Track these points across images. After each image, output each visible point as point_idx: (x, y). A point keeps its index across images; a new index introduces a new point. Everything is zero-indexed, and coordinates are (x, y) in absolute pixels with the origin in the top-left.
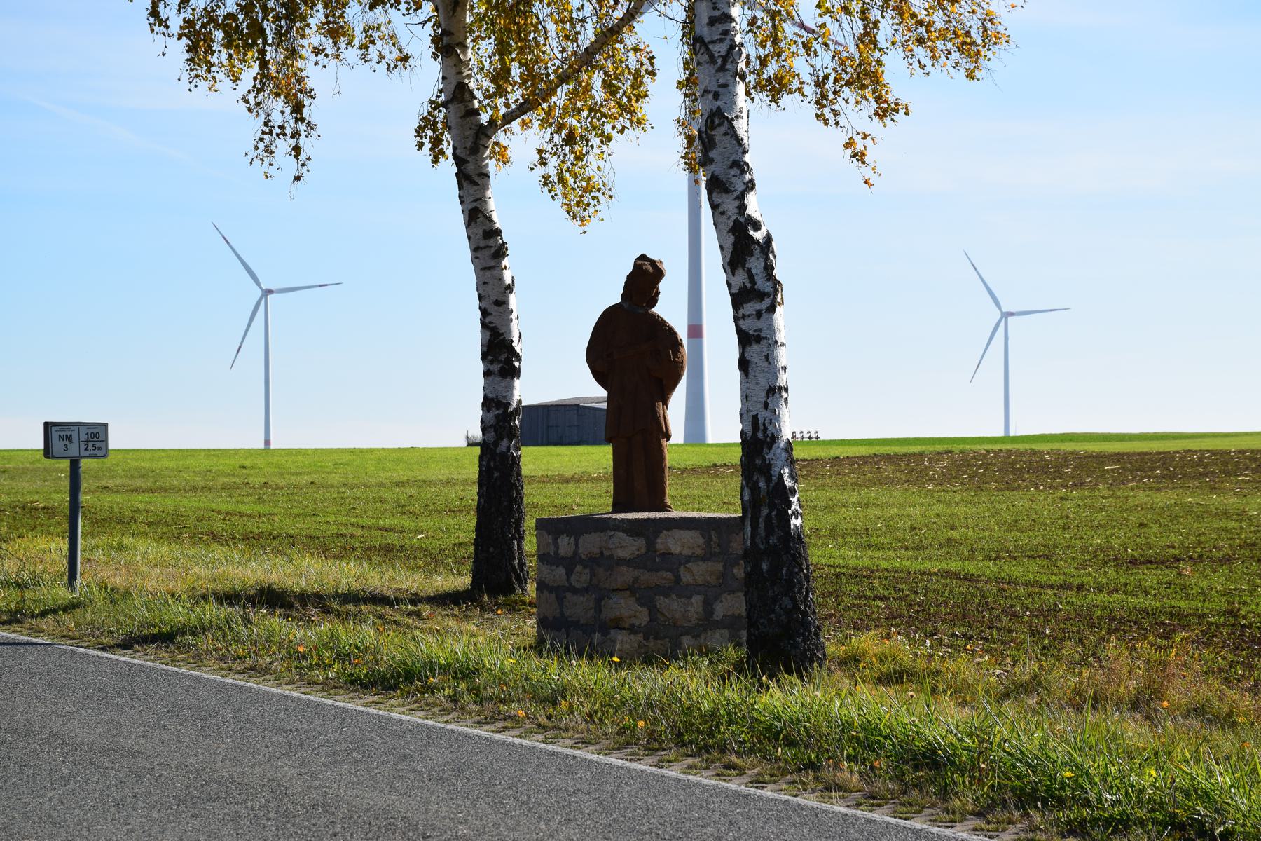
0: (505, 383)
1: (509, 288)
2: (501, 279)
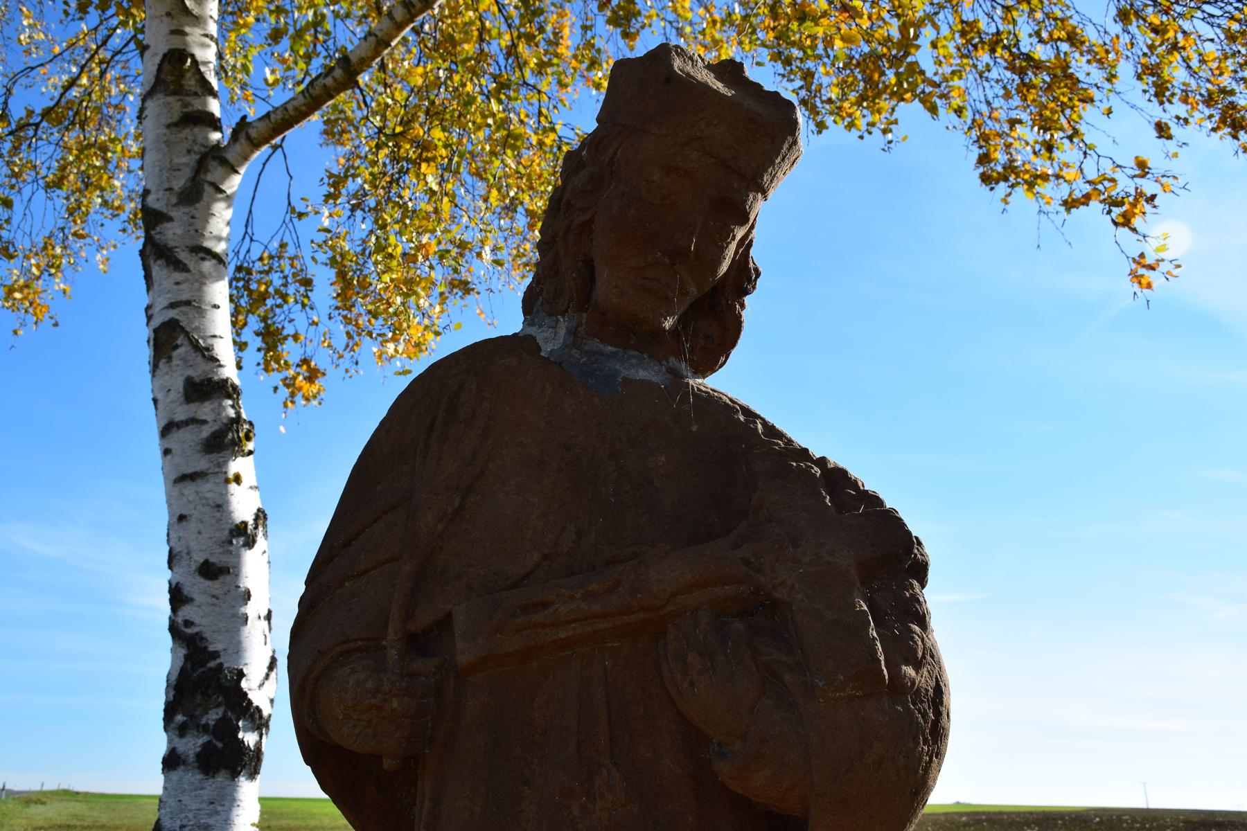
0: (211, 787)
1: (244, 535)
2: (221, 506)
